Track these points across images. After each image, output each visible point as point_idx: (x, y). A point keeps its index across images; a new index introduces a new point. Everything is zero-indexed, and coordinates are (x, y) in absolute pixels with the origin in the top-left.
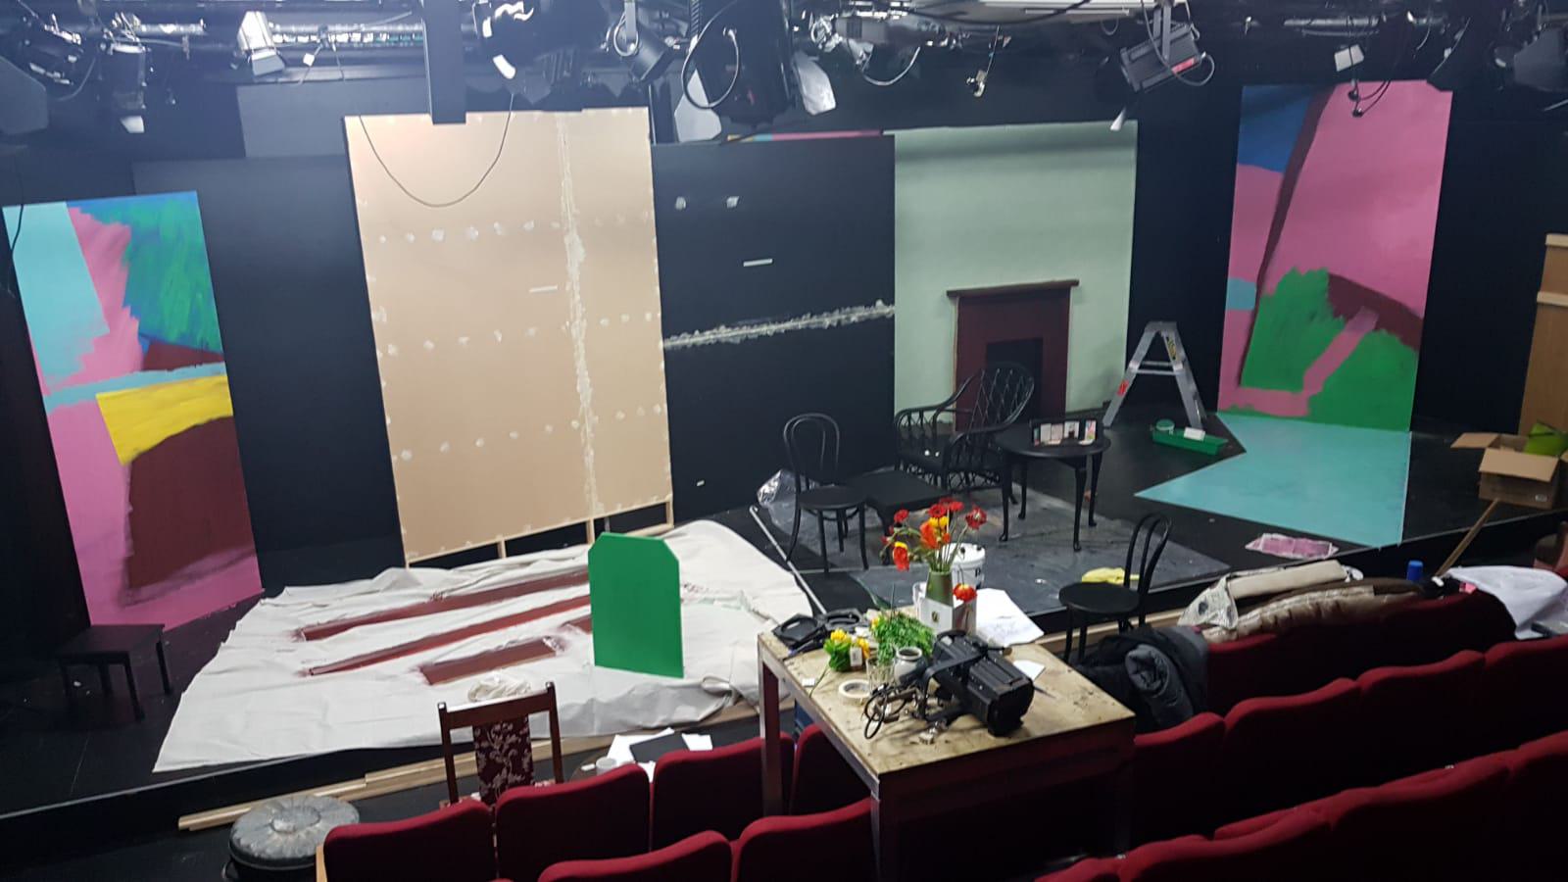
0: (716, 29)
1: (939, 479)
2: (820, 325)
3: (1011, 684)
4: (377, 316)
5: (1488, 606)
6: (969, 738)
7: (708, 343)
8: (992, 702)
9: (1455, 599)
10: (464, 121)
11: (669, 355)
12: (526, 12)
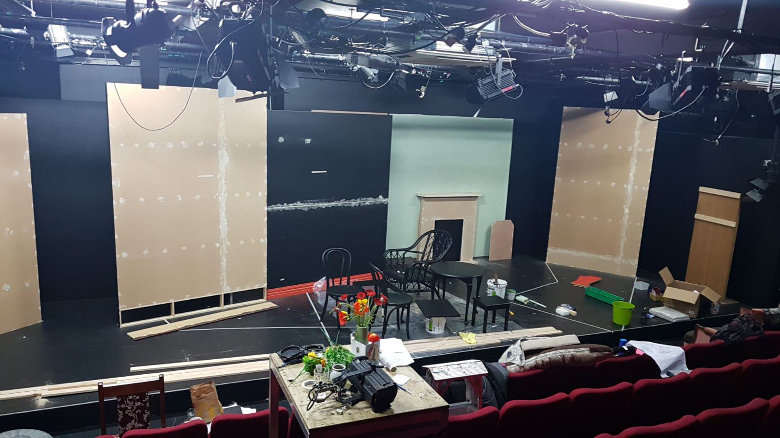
0: (226, 43)
1: (402, 285)
2: (350, 205)
3: (384, 385)
4: (116, 183)
5: (647, 361)
6: (363, 412)
7: (291, 209)
8: (374, 394)
9: (633, 357)
10: (158, 88)
11: (272, 217)
12: (128, 24)
